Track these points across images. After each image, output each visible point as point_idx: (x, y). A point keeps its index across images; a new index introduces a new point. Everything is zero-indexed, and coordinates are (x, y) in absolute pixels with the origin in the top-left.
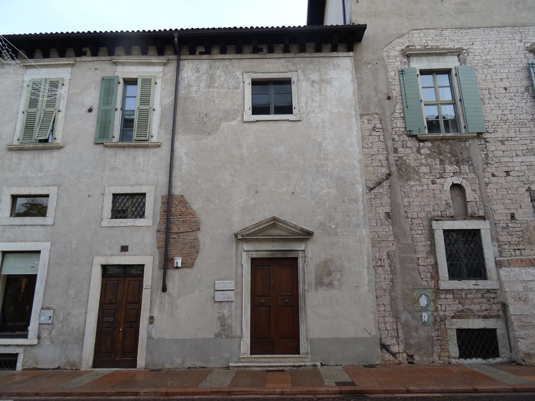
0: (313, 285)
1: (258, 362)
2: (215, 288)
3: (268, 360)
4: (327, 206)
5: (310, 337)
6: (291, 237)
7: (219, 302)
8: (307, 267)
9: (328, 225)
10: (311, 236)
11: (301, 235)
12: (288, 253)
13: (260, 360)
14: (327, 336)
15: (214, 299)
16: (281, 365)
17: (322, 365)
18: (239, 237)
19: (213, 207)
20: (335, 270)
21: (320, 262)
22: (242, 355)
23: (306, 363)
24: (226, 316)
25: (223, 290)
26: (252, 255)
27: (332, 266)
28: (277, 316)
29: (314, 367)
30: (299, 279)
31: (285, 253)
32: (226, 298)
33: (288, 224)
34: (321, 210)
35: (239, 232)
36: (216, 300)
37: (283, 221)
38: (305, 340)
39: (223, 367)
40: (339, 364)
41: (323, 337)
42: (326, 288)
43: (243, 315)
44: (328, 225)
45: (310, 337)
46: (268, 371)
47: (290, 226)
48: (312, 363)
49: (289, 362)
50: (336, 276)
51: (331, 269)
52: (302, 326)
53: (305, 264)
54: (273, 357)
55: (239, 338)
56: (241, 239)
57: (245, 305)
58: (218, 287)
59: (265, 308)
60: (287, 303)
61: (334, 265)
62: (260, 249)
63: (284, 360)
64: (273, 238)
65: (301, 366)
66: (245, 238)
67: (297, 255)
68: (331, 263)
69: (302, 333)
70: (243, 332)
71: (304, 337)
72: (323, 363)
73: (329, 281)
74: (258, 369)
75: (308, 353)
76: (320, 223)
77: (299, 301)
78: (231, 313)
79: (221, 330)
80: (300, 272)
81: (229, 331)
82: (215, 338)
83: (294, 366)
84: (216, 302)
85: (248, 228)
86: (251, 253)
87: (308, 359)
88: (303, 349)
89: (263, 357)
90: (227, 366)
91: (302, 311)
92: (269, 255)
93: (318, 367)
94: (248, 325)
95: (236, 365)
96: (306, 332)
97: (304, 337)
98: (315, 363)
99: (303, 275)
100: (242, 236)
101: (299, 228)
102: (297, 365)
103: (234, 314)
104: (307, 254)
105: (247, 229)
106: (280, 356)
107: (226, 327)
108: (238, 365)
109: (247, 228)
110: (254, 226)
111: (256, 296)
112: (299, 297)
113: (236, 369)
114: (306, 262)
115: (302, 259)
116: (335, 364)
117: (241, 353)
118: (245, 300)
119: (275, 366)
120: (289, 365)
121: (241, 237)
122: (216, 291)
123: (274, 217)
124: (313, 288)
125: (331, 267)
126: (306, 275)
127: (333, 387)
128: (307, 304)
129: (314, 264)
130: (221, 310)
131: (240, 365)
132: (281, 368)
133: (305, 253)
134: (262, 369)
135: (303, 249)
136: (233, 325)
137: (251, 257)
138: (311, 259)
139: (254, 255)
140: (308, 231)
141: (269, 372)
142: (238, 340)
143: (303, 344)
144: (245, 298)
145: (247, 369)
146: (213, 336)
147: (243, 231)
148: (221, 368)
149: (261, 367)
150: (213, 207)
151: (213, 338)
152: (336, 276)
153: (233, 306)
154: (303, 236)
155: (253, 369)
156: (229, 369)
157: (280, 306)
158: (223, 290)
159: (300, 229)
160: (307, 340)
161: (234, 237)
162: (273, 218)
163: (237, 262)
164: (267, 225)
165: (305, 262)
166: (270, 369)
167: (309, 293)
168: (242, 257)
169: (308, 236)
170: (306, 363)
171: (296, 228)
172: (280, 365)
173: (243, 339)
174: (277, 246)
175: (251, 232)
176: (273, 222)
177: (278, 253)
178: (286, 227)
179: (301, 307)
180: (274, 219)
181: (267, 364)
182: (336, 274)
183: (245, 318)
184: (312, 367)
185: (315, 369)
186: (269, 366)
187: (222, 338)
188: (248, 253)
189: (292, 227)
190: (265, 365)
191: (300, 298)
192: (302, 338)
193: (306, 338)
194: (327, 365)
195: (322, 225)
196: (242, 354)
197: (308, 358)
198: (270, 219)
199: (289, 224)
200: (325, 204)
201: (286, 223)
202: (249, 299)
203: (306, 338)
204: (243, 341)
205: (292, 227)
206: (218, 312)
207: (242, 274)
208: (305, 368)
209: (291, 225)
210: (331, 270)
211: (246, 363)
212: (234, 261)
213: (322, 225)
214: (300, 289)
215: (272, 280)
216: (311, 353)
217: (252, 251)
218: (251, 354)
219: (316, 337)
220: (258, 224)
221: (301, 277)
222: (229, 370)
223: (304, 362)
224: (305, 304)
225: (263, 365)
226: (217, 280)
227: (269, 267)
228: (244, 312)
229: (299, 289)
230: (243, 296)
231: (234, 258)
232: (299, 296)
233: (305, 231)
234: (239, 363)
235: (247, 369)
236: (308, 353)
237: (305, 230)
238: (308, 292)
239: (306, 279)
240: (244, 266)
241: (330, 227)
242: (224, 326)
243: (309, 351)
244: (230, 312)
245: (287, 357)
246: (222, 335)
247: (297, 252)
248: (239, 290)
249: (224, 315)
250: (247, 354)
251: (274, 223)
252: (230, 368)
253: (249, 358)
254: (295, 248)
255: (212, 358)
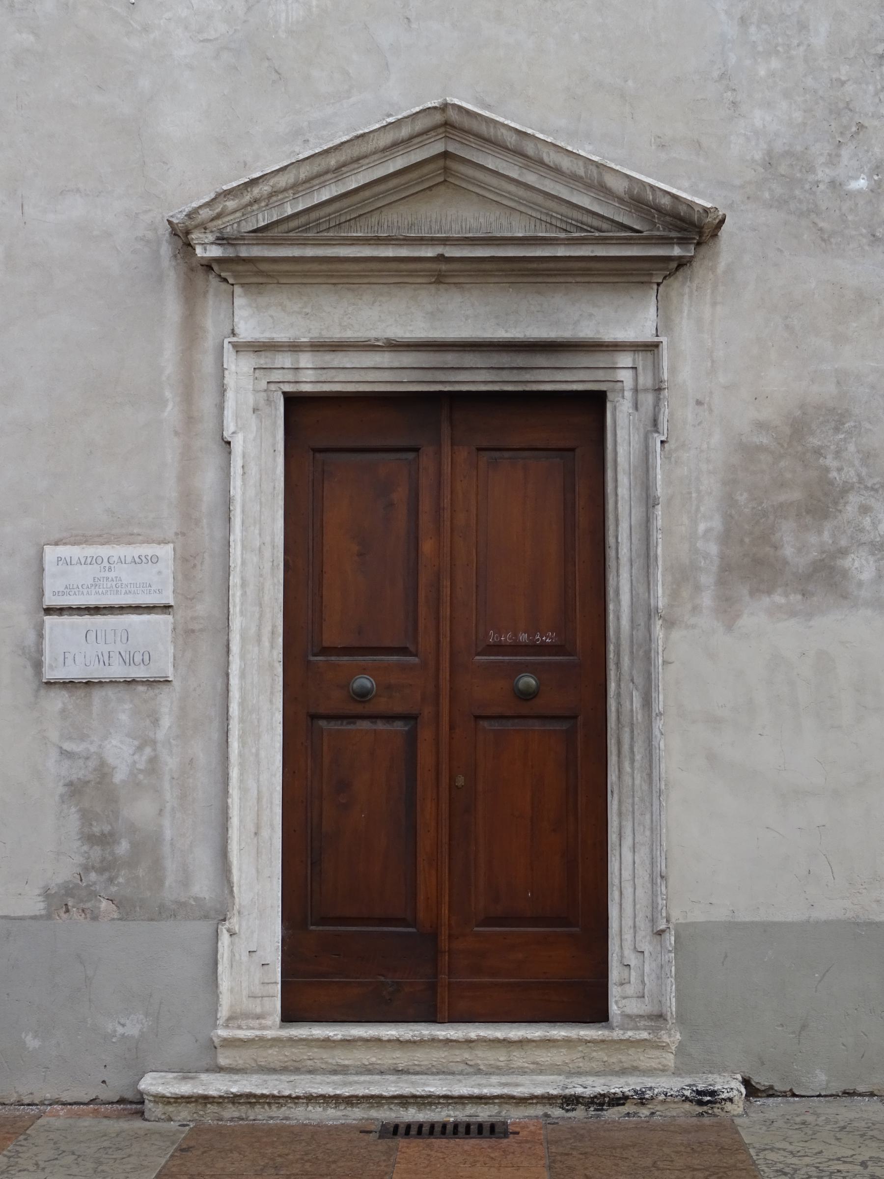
0: (707, 579)
1: (334, 1072)
2: (43, 595)
3: (401, 1058)
4: (819, 39)
5: (677, 916)
6: (561, 252)
7: (68, 684)
8: (667, 457)
9: (820, 175)
10: (703, 249)
11: (635, 237)
12: (541, 360)
13: (343, 1057)
14: (792, 913)
15: (38, 665)
16: (486, 1091)
17: (752, 1090)
18: (199, 251)
19: (27, 38)
20: (861, 480)
21: (761, 426)
22: (227, 1027)
23: (649, 1082)
24: (119, 777)
25: (96, 610)
26: (290, 376)
27: (838, 454)
28: (460, 781)
29: (700, 1109)
30: (611, 540)
31: (520, 360)
32: (116, 660)
33: (541, 163)
34: (775, 64)
35: (206, 214)
36: (49, 674)
37: (511, 140)
38: (643, 925)
39: (103, 1097)
40: (861, 1089)
41: (762, 916)
42: (795, 598)
43: (234, 773)
44: (823, 174)
45: (677, 916)
46: (395, 1131)
47: (556, 171)
48: (688, 1081)
49: (540, 1069)
50: (867, 522)
51: (834, 474)
52: (627, 842)
53: (659, 438)
54: (433, 1041)
55: (206, 917)
56: (219, 260)
57: (242, 704)
58: (59, 586)
59: (380, 726)
60: (527, 696)
61: (852, 448)
62: (349, 335)
63: (500, 1057)
64: (441, 258)
65: (618, 1100)
66: (244, 252)
67: (600, 375)
68: (837, 430)
69: (628, 891)
70: (235, 877)
71: (640, 916)
72: (761, 1080)
73: (814, 554)
74: (332, 1115)
75: (660, 1017)
76: (769, 163)
77: (612, 687)
78: (153, 760)
79: (87, 868)
80: (623, 491)
81: (141, 872)
82: (49, 917)
83: (570, 1101)
84: (49, 684)
85: (265, 189)
86: (285, 360)
87: (657, 1053)
88: (630, 990)
89: (367, 1041)
90: (129, 1095)
91: (626, 747)
92: (405, 376)
93: (728, 1106)
94: (265, 833)
95: (185, 1089)
96: (653, 882)
97: (640, 916)
98: (711, 1078)
99: (637, 514)
100: (222, 240)
101: (618, 186)
102: (588, 1092)
103: (170, 762)
104: (673, 370)
105: (256, 191)
106: (474, 1031)
107: (123, 847)
108: (200, 1091)
109: (254, 182)
110: (304, 172)
111: (325, 651)
112: (611, 656)
113: (184, 1113)
114: (664, 425)
115: (636, 407)
116: (837, 1087)
117: (224, 1012)
118: (243, 675)
119: (446, 1097)
120: (539, 1091)
121: (215, 252)
122: (49, 611)
123: (444, 107)
124: (707, 600)
125: (830, 462)
126: (659, 511)
127: (657, 928)
128: (660, 702)
129: (716, 439)
130: (83, 738)
131: (212, 1092)
132: (484, 1114)
133: (656, 367)
134: (356, 1114)
135: (648, 336)
136: (168, 834)
137: (288, 388)
138: (699, 403)
139: (309, 375)
140: (682, 210)
141: (402, 1142)
142: (204, 928)
143: (632, 959)
144: (243, 657)
145: (261, 1114)
146: (37, 907)
147: (231, 204)
148: (92, 1101)
149: (351, 1101)
150: (27, 38)
151: (34, 918)
152: (867, 522)
153: (165, 710)
154: (649, 241)
155: (300, 1114)
156: (141, 1114)
157: (477, 718)
158: (96, 610)
159: (629, 192)
160: (660, 933)
161: (166, 250)
162: (438, 118)
163: (190, 419)
164: (399, 163)
165: (655, 422)
166: (412, 1115)
167: (676, 635)
168: (222, 390)
169: (682, 242)
170: (649, 1082)
171: (602, 190)
172: (476, 1091)
173: (234, 922)
174: (544, 980)
175: (289, 211)
176: (438, 148)
177: (469, 359)
178: (531, 178)
179: (625, 719)
180: (446, 124)
181: (391, 1087)
182: (865, 510)
183: (244, 790)
184: (687, 1106)
185: (706, 1120)
186: (404, 1100)
187: (95, 918)
188: (263, 360)
189: (573, 179)
190: (375, 1091)
191: (618, 664)
192: (628, 922)
193: (653, 921)
194: (784, 1095)
195: (783, 169)
196: (230, 1019)
197: (664, 1048)
198: (420, 125)
199: (550, 157)
200: (803, 27)
201: (530, 149)
202: (271, 667)
203: (653, 921)
204: (232, 934)
205: (573, 179)
206: (66, 754)
207: (228, 502)
208: (644, 1112)
209: (566, 163)
210: (831, 483)
211: (255, 1078)
212: (171, 412)
213: (783, 169)
214: (618, 602)
215: (427, 546)
216: (681, 1019)
217: (294, 347)
218: (289, 1016)
219: (720, 914)
220: (332, 161)
221: (624, 526)
222: (138, 1124)
223: (634, 1070)
224: (647, 703)
225: (361, 1091)
226: (56, 544)
227: (411, 456)
228: (241, 755)
229: (611, 607)
230: (235, 648)
231: (168, 394)
232: (611, 648)
233: (659, 209)
234: (204, 1077)
235: (261, 1114)
236: (660, 1017)
237: (665, 201)
238: (670, 624)
239: (658, 537)
240: (238, 446)
241: (834, 185)
242: (105, 840)
243: (671, 1005)
244: (148, 751)
245: (522, 1043)
246: (94, 895)
247: (601, 359)
248: (205, 607)
249: (103, 772)
250: (258, 1017)
251: (445, 155)
252: (149, 1105)
253: (276, 1042)
254: (586, 332)
255: (32, 1042)
